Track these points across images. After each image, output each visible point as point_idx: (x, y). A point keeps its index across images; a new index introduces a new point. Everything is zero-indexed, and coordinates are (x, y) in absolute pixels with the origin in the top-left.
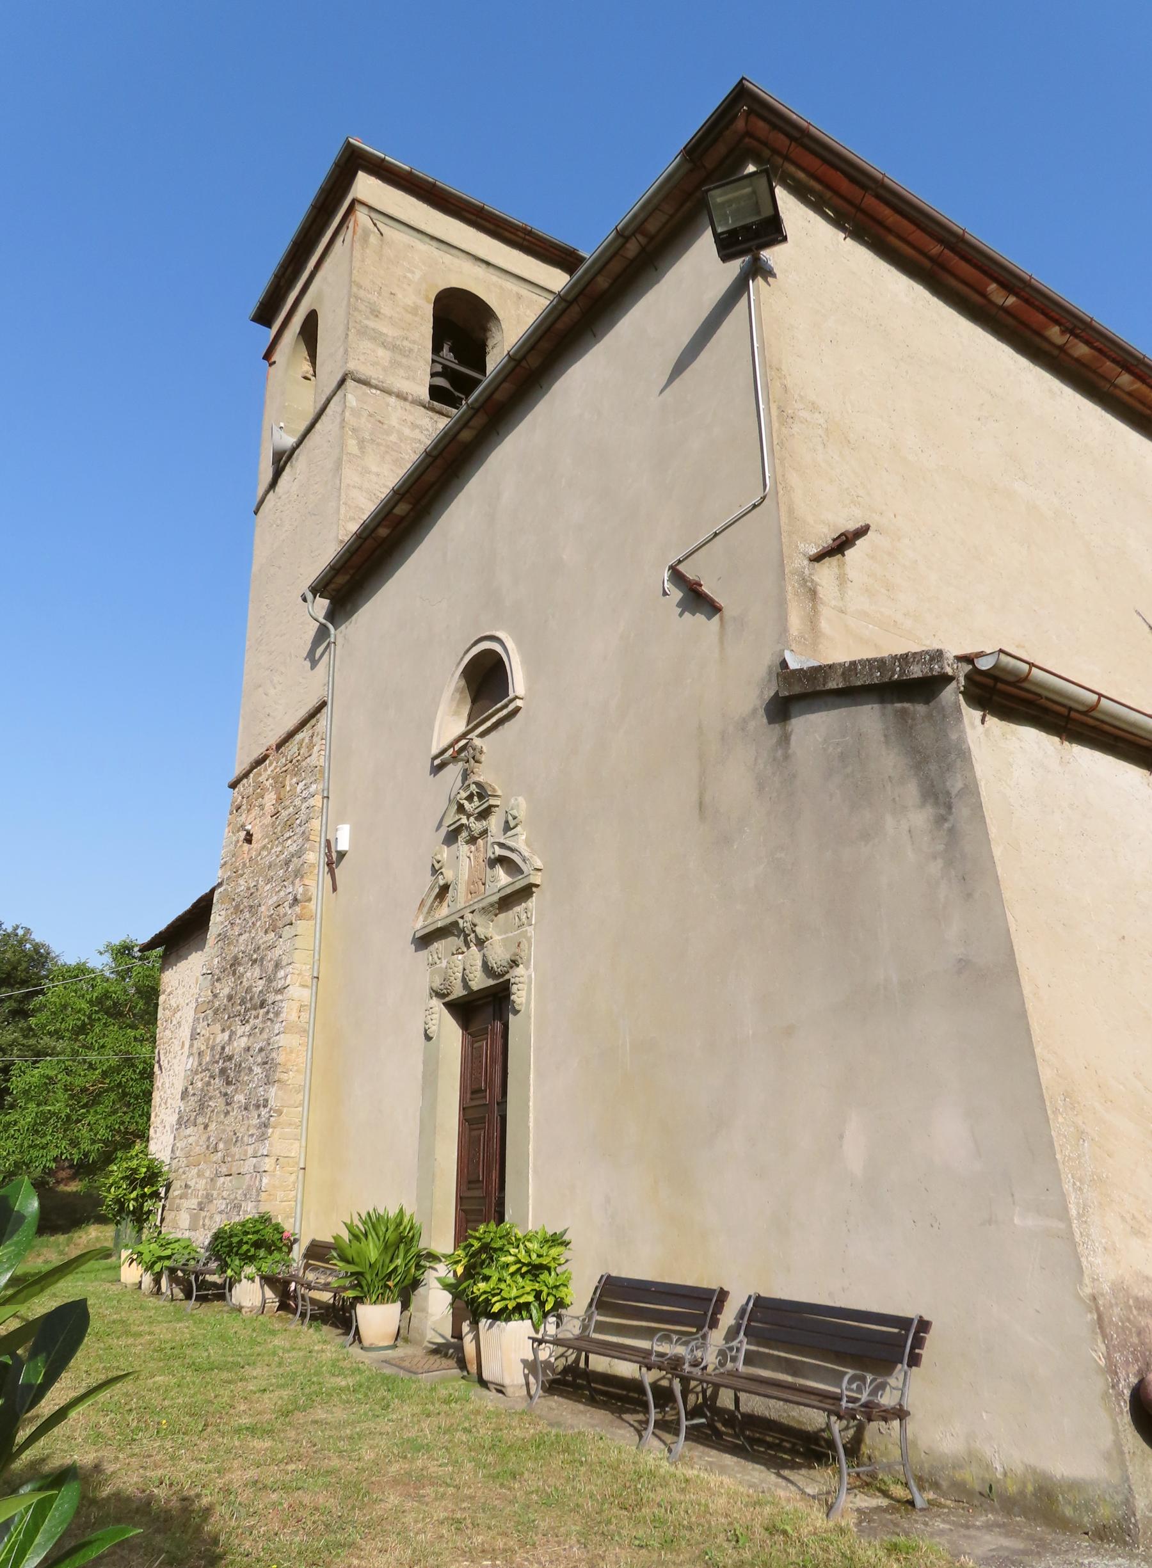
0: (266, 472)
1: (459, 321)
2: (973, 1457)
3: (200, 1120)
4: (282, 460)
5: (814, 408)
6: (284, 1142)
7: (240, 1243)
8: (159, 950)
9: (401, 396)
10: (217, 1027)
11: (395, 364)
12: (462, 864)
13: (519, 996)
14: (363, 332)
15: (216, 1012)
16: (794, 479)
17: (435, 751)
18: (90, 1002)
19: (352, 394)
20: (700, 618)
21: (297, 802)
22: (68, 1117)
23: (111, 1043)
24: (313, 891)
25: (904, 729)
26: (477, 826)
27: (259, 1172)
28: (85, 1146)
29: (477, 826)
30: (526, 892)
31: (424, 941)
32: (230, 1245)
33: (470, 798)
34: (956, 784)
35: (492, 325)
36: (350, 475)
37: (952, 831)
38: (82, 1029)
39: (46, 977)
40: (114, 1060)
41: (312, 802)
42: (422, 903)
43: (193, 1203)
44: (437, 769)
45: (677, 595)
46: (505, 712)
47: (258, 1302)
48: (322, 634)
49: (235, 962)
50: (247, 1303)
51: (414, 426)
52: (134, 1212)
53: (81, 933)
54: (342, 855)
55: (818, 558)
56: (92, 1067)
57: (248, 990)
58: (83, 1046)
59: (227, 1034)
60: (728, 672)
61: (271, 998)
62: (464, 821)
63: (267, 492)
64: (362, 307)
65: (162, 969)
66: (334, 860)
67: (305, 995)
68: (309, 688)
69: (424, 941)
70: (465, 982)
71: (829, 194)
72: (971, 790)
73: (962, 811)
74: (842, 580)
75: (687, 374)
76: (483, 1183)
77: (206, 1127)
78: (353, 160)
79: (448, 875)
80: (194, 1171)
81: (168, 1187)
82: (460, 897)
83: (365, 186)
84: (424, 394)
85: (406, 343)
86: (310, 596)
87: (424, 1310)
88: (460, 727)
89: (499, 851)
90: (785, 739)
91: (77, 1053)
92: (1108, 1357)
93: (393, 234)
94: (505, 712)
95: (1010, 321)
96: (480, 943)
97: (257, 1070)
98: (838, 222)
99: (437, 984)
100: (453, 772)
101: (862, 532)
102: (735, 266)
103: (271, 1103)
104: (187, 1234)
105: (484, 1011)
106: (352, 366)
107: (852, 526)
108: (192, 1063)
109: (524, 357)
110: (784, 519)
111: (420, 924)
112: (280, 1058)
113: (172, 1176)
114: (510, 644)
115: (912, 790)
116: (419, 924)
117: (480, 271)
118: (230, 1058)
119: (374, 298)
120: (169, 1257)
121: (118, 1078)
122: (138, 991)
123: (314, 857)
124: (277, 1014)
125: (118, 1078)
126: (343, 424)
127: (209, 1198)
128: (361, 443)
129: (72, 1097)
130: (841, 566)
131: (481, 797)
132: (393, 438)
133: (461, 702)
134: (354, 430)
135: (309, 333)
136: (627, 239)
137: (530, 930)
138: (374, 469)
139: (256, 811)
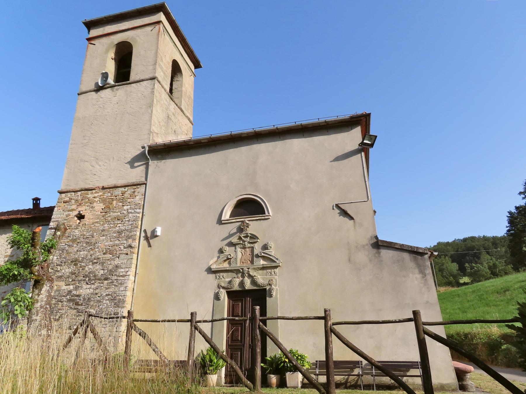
37: (426, 280)
46: (263, 218)
54: (157, 236)
60: (357, 234)
78: (160, 8)
90: (379, 253)
94: (263, 218)
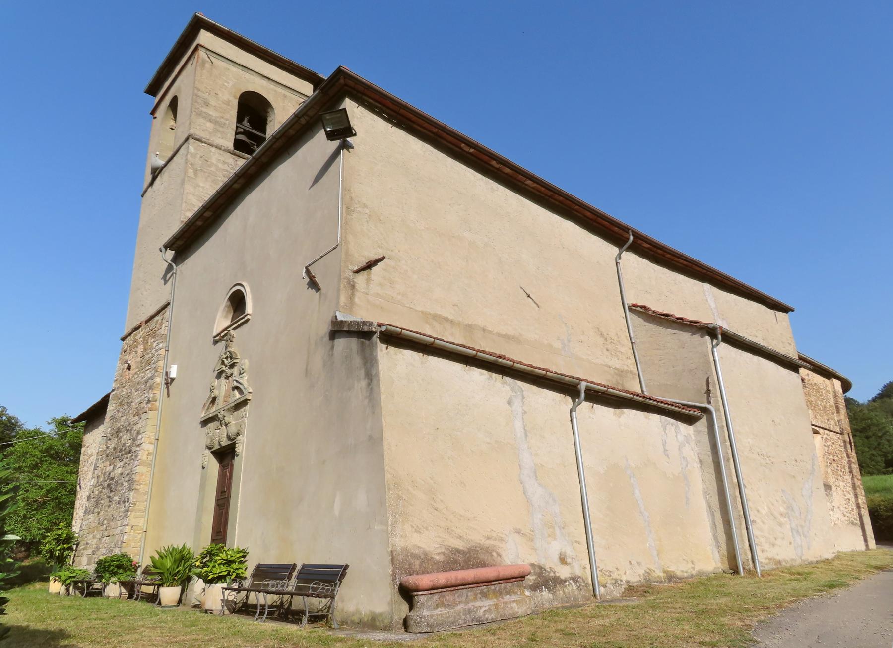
0: (149, 178)
1: (252, 108)
2: (358, 611)
3: (96, 510)
4: (156, 172)
5: (365, 206)
6: (136, 519)
7: (110, 565)
8: (84, 423)
9: (218, 147)
10: (108, 463)
11: (215, 130)
12: (223, 387)
13: (238, 449)
14: (200, 114)
15: (107, 456)
16: (350, 238)
17: (215, 334)
18: (41, 451)
19: (192, 146)
20: (314, 291)
21: (153, 351)
22: (25, 515)
23: (53, 473)
24: (158, 396)
25: (362, 349)
26: (229, 371)
27: (123, 533)
28: (34, 532)
29: (229, 371)
30: (244, 403)
31: (205, 423)
32: (104, 567)
33: (227, 358)
34: (374, 372)
35: (269, 110)
36: (188, 188)
38: (36, 466)
39: (15, 436)
40: (54, 484)
41: (160, 352)
42: (204, 406)
43: (90, 552)
44: (216, 342)
45: (307, 280)
47: (117, 594)
48: (170, 268)
49: (118, 431)
50: (112, 595)
51: (224, 163)
52: (58, 557)
53: (37, 415)
54: (173, 379)
55: (357, 272)
56: (41, 488)
57: (124, 445)
58: (36, 476)
59: (112, 467)
60: (317, 316)
61: (134, 448)
62: (224, 368)
63: (148, 187)
64: (199, 101)
65: (85, 433)
66: (169, 381)
67: (151, 447)
68: (162, 294)
69: (205, 423)
70: (220, 444)
71: (384, 108)
72: (377, 374)
73: (374, 382)
74: (368, 280)
75: (325, 178)
76: (220, 532)
77: (99, 513)
78: (197, 25)
79: (216, 393)
80: (91, 536)
81: (78, 545)
82: (220, 403)
83: (205, 37)
84: (230, 145)
85: (222, 120)
86: (163, 249)
87: (192, 590)
88: (228, 323)
89: (236, 384)
90: (333, 347)
91: (32, 480)
92: (393, 571)
93: (218, 62)
95: (473, 158)
96: (226, 425)
97: (125, 484)
98: (389, 120)
99: (208, 444)
100: (222, 344)
101: (383, 258)
102: (337, 143)
103: (131, 500)
104: (86, 567)
105: (225, 454)
106: (192, 131)
107: (374, 256)
108: (93, 482)
109: (260, 157)
110: (343, 256)
111: (203, 415)
112: (136, 478)
113: (80, 539)
114: (248, 289)
115: (362, 372)
116: (203, 415)
117: (265, 82)
118: (113, 479)
119: (206, 96)
120: (74, 577)
121: (56, 494)
122: (71, 445)
123: (159, 380)
124: (136, 457)
125: (56, 494)
126: (186, 161)
127: (98, 548)
128: (196, 172)
129: (27, 504)
130: (369, 275)
131: (231, 358)
132: (213, 169)
133: (228, 312)
134: (192, 164)
135: (174, 105)
136: (300, 118)
137: (246, 420)
138: (202, 185)
139: (133, 354)
